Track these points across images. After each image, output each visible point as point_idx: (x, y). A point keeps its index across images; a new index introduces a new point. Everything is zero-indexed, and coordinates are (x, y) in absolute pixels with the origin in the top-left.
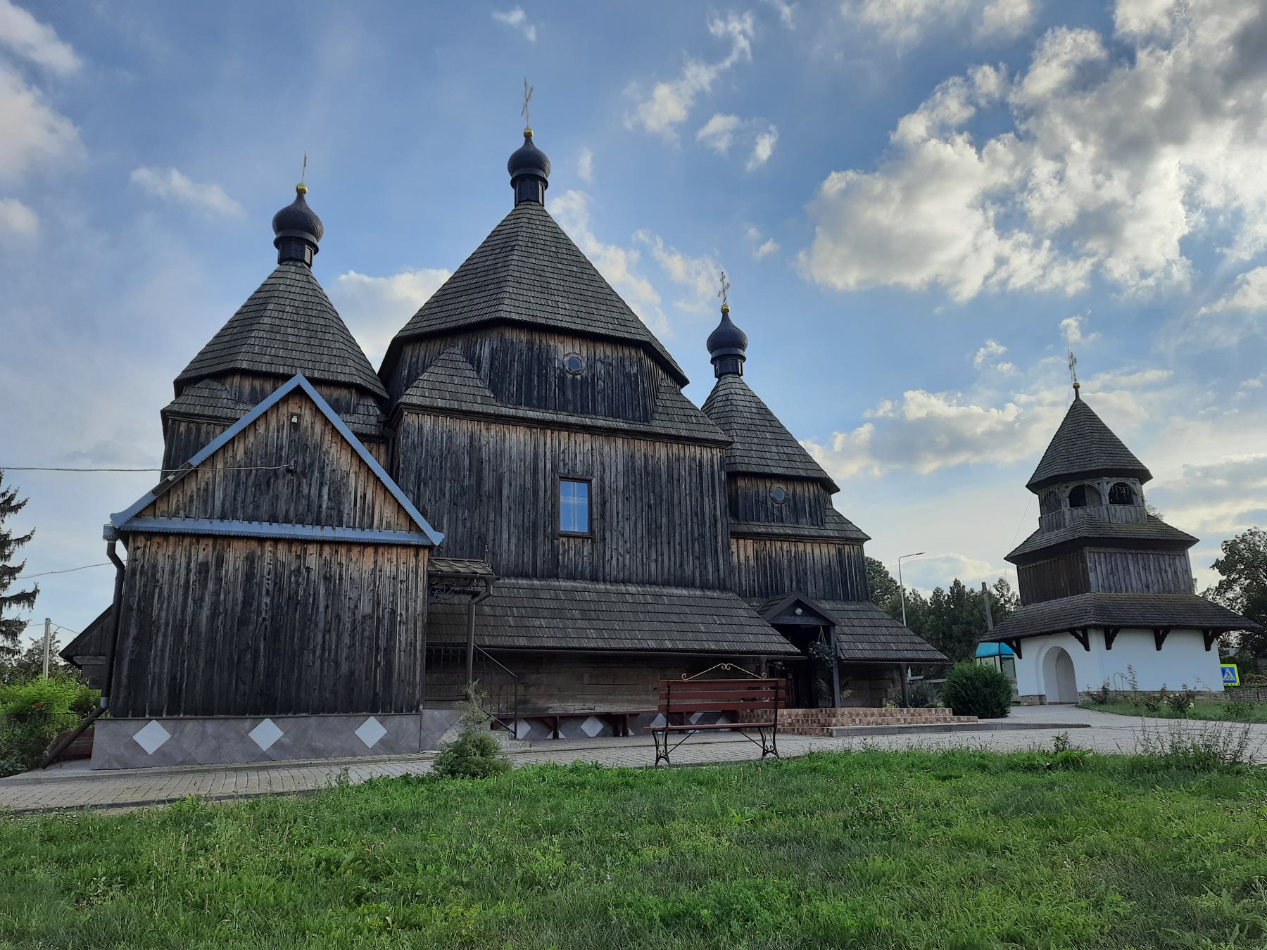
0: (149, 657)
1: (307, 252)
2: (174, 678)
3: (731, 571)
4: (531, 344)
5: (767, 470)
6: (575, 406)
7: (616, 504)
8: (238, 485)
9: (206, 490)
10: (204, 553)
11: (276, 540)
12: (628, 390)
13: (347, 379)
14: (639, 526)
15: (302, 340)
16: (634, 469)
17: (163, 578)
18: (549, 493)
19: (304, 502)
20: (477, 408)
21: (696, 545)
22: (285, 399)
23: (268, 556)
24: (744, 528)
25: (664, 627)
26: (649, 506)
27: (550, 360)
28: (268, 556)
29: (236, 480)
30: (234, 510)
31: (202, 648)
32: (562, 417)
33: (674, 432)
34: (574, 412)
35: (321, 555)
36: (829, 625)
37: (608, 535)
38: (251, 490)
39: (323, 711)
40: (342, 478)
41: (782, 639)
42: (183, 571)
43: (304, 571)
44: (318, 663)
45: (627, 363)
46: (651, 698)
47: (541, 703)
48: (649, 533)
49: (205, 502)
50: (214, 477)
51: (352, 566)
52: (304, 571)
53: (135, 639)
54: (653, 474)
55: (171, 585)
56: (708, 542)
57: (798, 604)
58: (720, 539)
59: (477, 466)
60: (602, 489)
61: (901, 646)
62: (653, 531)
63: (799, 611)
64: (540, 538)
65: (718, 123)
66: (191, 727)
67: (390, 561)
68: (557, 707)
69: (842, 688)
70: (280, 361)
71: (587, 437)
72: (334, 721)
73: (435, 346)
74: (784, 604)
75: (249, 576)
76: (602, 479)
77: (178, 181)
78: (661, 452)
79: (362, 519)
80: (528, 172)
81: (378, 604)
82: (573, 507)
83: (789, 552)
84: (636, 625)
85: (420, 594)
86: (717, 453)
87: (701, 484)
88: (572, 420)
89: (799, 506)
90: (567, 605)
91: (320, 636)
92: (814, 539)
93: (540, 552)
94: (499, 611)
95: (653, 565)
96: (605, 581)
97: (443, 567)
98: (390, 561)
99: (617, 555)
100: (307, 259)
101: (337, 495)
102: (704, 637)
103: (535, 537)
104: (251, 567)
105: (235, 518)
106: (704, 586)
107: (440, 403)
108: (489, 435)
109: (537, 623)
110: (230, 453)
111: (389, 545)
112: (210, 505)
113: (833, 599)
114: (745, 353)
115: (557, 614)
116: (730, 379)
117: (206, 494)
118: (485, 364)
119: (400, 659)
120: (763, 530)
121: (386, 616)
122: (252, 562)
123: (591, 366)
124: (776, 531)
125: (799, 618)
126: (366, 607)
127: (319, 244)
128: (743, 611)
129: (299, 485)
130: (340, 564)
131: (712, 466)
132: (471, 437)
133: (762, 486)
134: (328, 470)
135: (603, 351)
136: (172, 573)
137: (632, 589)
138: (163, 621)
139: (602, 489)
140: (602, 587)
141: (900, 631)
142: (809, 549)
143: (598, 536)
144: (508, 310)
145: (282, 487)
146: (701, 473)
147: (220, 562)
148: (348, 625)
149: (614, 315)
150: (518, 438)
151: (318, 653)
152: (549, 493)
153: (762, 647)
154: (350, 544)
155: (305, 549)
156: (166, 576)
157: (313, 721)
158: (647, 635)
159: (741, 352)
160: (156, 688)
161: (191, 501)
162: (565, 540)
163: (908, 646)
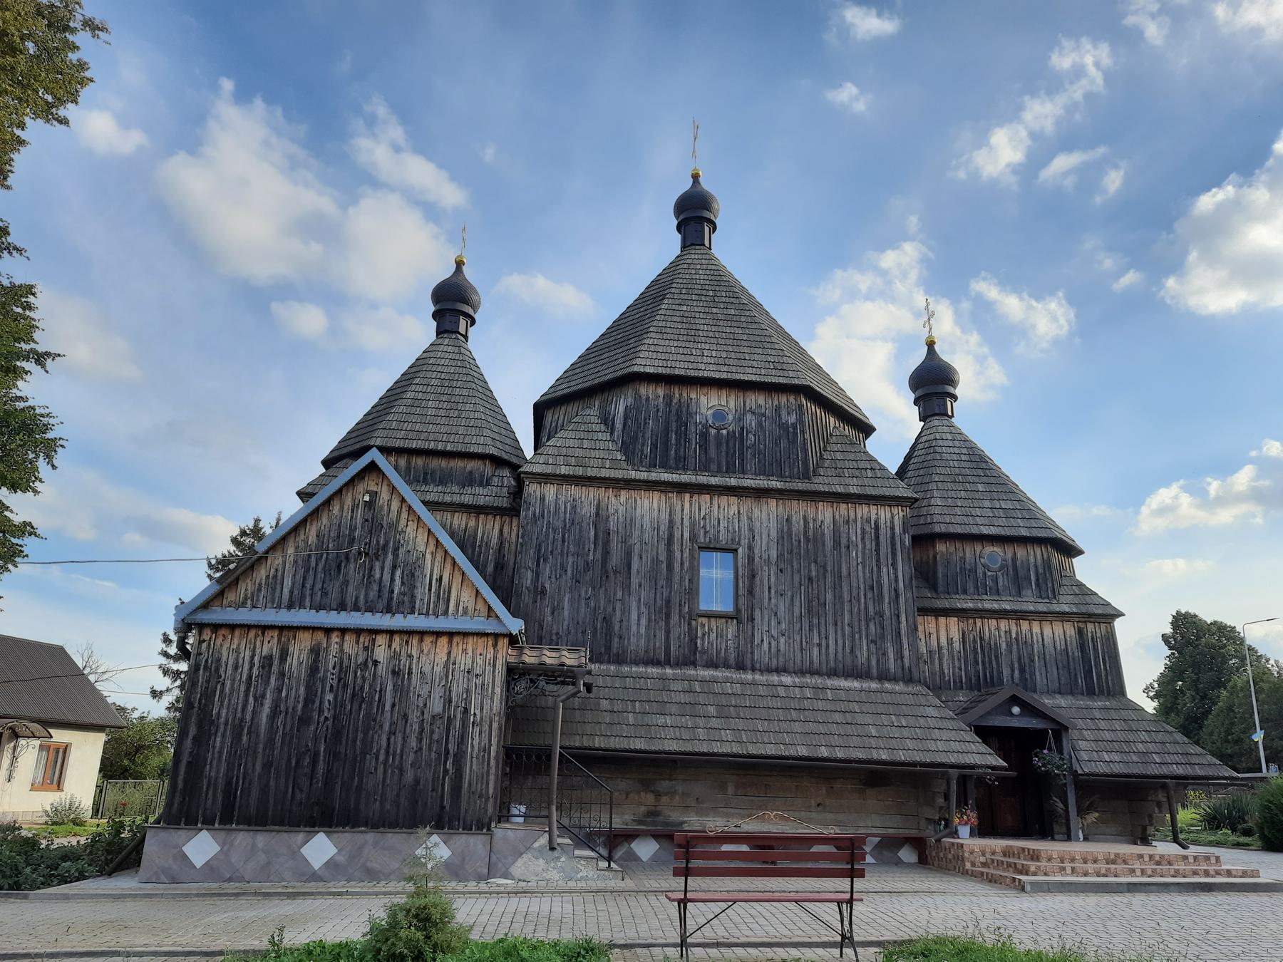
0: (206, 759)
1: (462, 323)
2: (229, 783)
3: (919, 658)
4: (668, 399)
5: (975, 530)
6: (719, 466)
7: (767, 576)
8: (307, 571)
9: (275, 577)
10: (269, 645)
11: (343, 631)
12: (784, 443)
13: (480, 450)
14: (797, 603)
15: (442, 413)
16: (790, 534)
17: (227, 673)
18: (686, 565)
19: (375, 587)
20: (604, 473)
21: (872, 626)
22: (361, 475)
23: (334, 649)
24: (945, 603)
25: (822, 728)
26: (810, 579)
27: (690, 414)
28: (334, 649)
29: (305, 566)
30: (303, 597)
31: (260, 750)
32: (703, 479)
33: (840, 489)
34: (718, 472)
35: (390, 646)
36: (1060, 730)
37: (757, 614)
38: (320, 575)
39: (384, 826)
40: (418, 559)
41: (983, 748)
42: (246, 666)
43: (370, 664)
44: (381, 769)
45: (784, 412)
46: (814, 815)
47: (675, 816)
48: (810, 610)
49: (274, 590)
50: (284, 563)
51: (423, 658)
52: (370, 664)
53: (194, 739)
54: (815, 540)
55: (233, 680)
56: (887, 623)
57: (1014, 700)
58: (903, 618)
59: (603, 538)
60: (751, 559)
61: (1168, 759)
62: (814, 608)
63: (1016, 710)
64: (675, 618)
65: (1063, 163)
66: (242, 839)
67: (465, 651)
68: (694, 822)
69: (1081, 812)
70: (414, 435)
71: (733, 499)
72: (394, 838)
73: (573, 408)
74: (993, 701)
75: (314, 670)
76: (750, 548)
77: (541, 282)
78: (825, 513)
79: (436, 605)
80: (694, 214)
81: (450, 701)
82: (716, 583)
83: (1008, 632)
84: (785, 726)
85: (498, 690)
86: (899, 513)
87: (878, 550)
88: (714, 481)
89: (1021, 573)
90: (702, 699)
91: (384, 738)
92: (1042, 616)
93: (675, 633)
94: (618, 706)
95: (816, 651)
96: (753, 669)
97: (530, 657)
98: (465, 651)
99: (770, 636)
100: (462, 330)
101: (411, 579)
102: (873, 743)
103: (668, 617)
104: (316, 660)
105: (302, 606)
106: (883, 677)
107: (564, 470)
108: (618, 503)
109: (661, 720)
110: (302, 537)
111: (465, 634)
112: (277, 594)
113: (1072, 693)
114: (958, 392)
115: (689, 709)
116: (936, 422)
117: (275, 581)
118: (619, 425)
119: (471, 767)
120: (970, 605)
121: (458, 716)
122: (318, 655)
123: (740, 419)
124: (987, 605)
125: (1016, 718)
126: (436, 706)
127: (476, 316)
128: (932, 709)
129: (371, 569)
130: (410, 656)
131: (892, 528)
132: (598, 506)
133: (969, 551)
134: (402, 551)
135: (756, 400)
136: (236, 667)
137: (787, 679)
138: (222, 720)
139: (751, 559)
140: (749, 676)
141: (1167, 738)
142: (1036, 629)
143: (744, 615)
144: (643, 364)
145: (353, 572)
146: (877, 537)
147: (284, 654)
148: (416, 727)
149: (771, 359)
150: (650, 506)
151: (382, 758)
152: (686, 565)
153: (953, 759)
154: (422, 634)
155: (374, 640)
156: (230, 671)
157: (370, 837)
158: (799, 738)
159: (951, 389)
160: (210, 793)
161: (259, 590)
162: (704, 620)
163: (1177, 758)
